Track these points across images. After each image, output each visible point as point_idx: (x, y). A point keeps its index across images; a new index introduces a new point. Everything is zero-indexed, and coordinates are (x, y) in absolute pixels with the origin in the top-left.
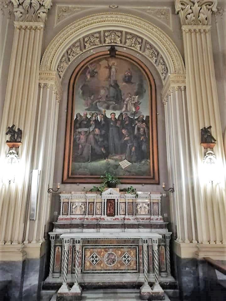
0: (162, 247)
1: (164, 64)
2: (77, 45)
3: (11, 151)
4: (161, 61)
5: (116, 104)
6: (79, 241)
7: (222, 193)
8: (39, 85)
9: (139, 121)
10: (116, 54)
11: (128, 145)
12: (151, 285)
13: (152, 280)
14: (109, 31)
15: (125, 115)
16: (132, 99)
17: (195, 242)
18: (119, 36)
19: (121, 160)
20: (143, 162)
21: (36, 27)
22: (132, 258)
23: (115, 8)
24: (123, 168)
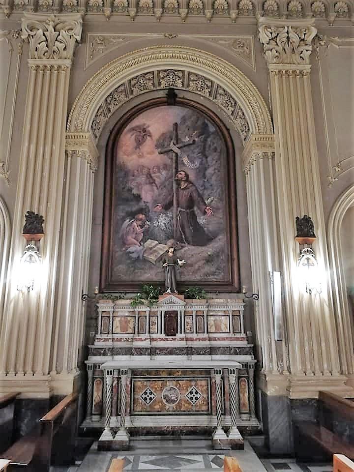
1: (244, 118)
2: (120, 90)
3: (29, 246)
4: (240, 113)
12: (226, 430)
13: (229, 424)
14: (165, 71)
17: (286, 373)
18: (180, 76)
22: (203, 396)
23: (172, 37)
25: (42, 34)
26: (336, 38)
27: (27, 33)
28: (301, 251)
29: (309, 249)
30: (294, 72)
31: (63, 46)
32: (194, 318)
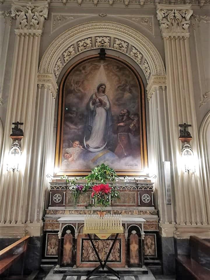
3: (15, 143)
7: (197, 181)
8: (37, 86)
17: (174, 223)
21: (34, 34)
25: (24, 14)
29: (188, 145)
30: (179, 37)
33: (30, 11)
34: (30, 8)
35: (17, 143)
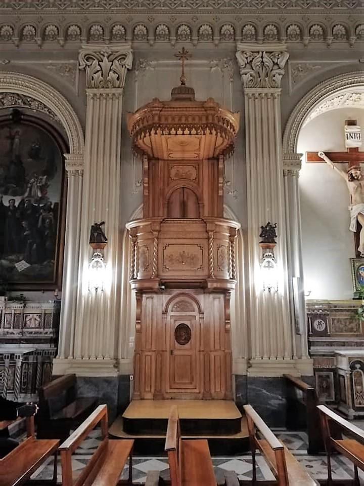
0: (47, 365)
5: (18, 188)
6: (19, 356)
9: (44, 210)
10: (21, 119)
11: (29, 241)
15: (27, 202)
16: (39, 180)
17: (70, 357)
19: (18, 261)
20: (45, 263)
24: (20, 271)
26: (153, 62)
27: (84, 63)
28: (263, 255)
31: (116, 76)
32: (13, 316)
33: (105, 59)
34: (106, 54)
35: (99, 254)
